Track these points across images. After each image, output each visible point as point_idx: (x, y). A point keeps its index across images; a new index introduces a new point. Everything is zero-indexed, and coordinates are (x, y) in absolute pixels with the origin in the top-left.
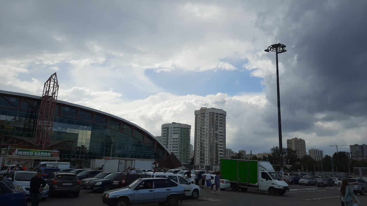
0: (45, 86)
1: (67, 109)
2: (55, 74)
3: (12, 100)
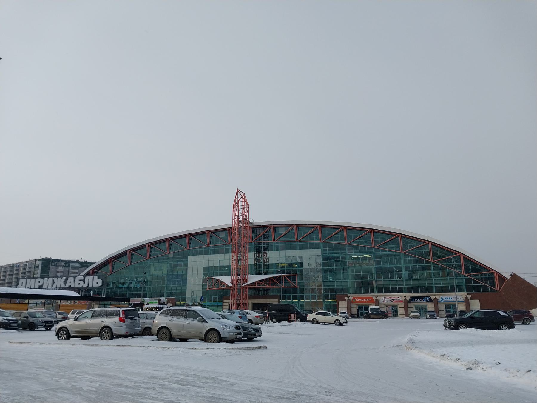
0: (248, 208)
1: (282, 231)
2: (238, 190)
3: (222, 235)
